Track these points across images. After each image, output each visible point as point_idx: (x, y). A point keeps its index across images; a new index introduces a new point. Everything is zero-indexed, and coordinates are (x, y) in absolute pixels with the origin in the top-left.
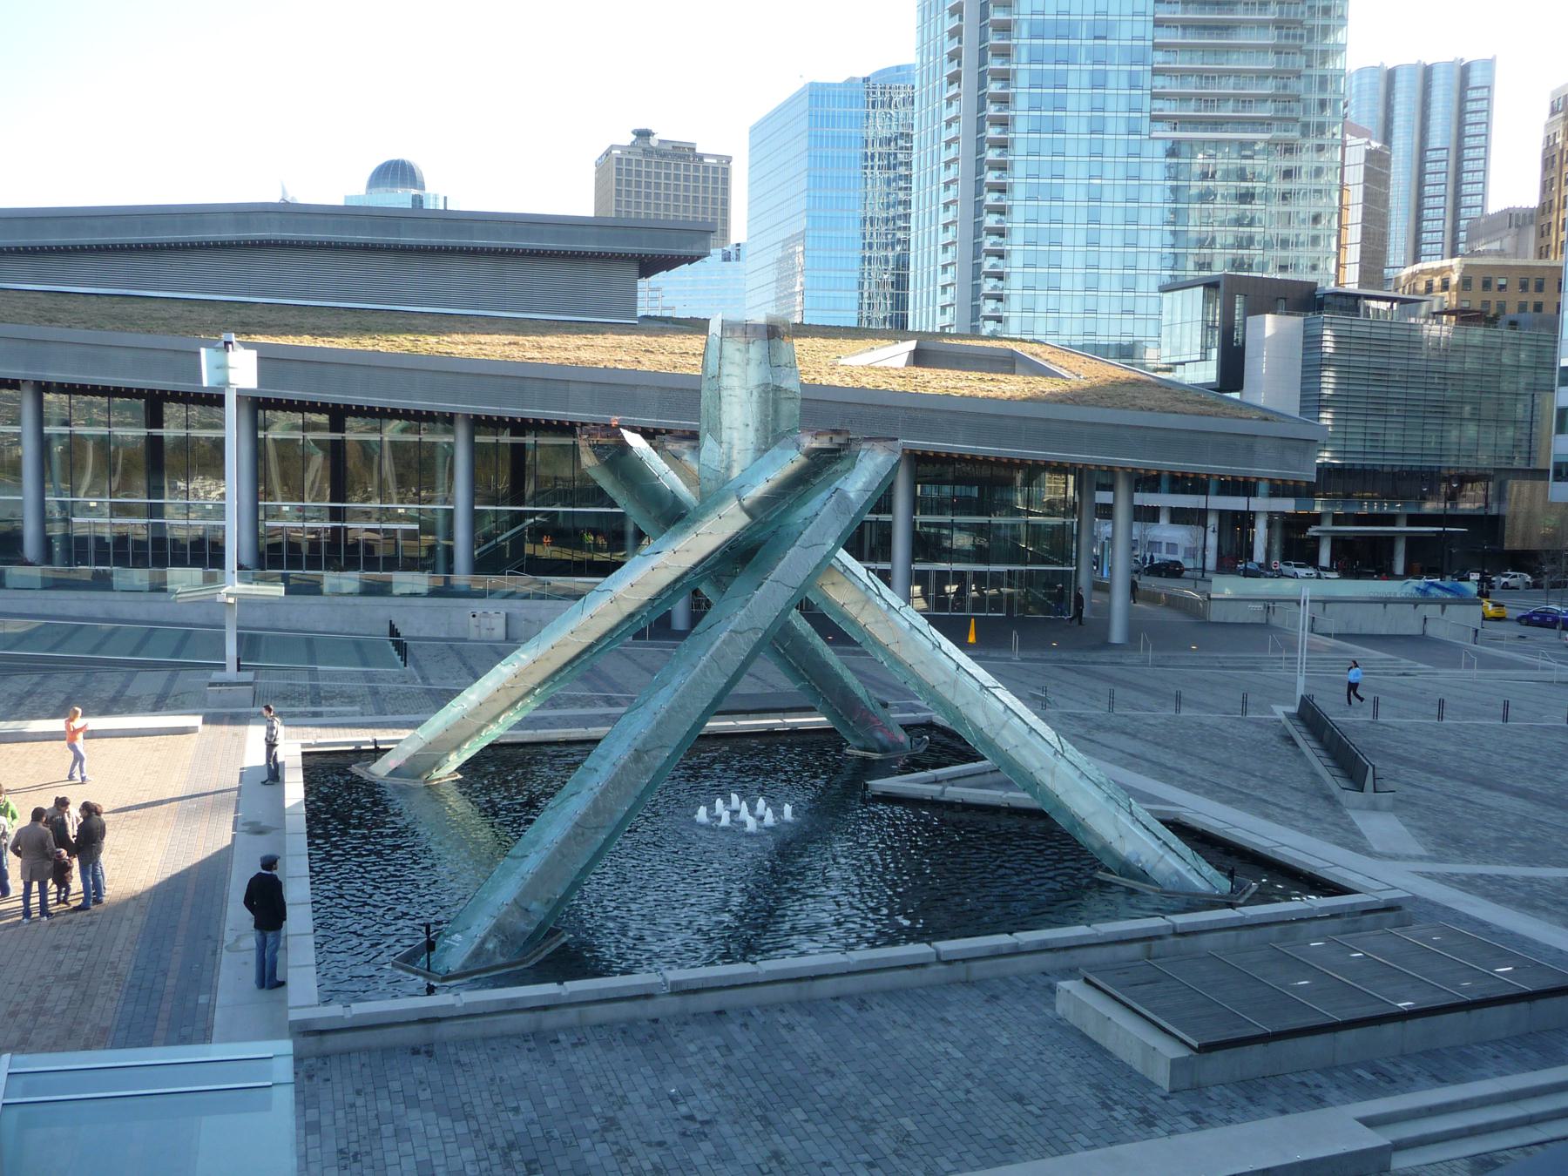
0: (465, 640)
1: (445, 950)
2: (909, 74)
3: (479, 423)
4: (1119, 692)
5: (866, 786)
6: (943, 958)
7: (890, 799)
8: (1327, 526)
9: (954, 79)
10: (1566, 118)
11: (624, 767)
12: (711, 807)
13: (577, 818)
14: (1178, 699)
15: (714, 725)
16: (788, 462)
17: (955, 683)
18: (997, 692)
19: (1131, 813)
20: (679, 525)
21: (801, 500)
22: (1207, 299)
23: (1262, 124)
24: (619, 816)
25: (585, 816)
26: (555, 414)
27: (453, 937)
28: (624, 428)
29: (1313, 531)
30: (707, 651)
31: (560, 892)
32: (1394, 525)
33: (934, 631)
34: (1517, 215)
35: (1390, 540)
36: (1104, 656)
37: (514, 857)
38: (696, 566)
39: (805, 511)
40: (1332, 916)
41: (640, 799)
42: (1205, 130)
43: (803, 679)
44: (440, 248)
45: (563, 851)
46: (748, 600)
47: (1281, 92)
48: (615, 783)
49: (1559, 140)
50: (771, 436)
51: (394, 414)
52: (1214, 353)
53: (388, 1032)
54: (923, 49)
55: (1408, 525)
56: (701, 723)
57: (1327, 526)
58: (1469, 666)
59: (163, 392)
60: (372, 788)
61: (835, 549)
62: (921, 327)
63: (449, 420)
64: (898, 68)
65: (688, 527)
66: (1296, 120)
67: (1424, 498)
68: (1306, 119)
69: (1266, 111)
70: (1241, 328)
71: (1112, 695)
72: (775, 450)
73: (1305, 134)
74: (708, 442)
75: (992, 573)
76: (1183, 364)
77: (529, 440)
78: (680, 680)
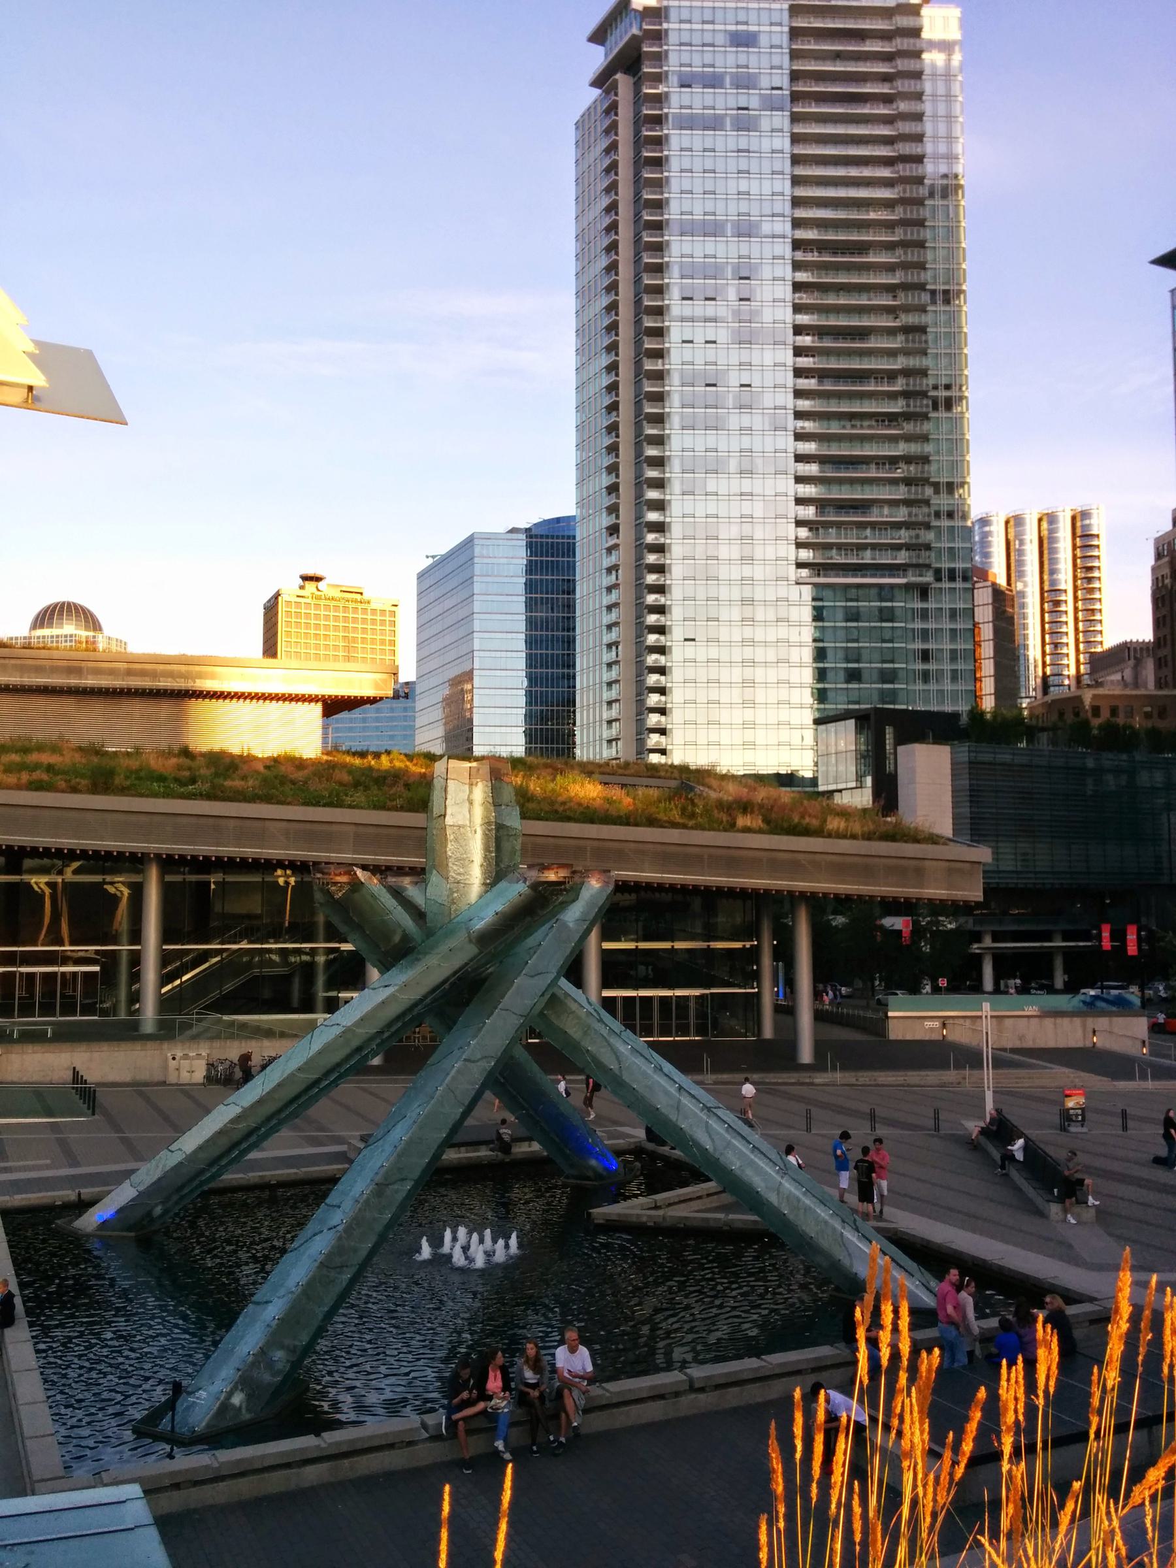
0: (164, 1083)
1: (188, 1408)
2: (569, 525)
3: (168, 863)
4: (815, 1111)
5: (589, 1214)
6: (697, 1385)
7: (613, 1227)
8: (988, 942)
9: (613, 530)
10: (1171, 563)
11: (367, 1202)
12: (437, 1242)
13: (321, 1258)
14: (872, 1117)
15: (452, 1156)
16: (514, 891)
17: (678, 1107)
18: (720, 1112)
19: (857, 1230)
20: (409, 958)
21: (529, 931)
22: (859, 730)
23: (898, 570)
24: (363, 1253)
25: (330, 1256)
26: (250, 851)
27: (197, 1394)
28: (356, 865)
29: (975, 948)
30: (443, 1081)
31: (304, 1338)
32: (1051, 941)
33: (655, 1054)
34: (1135, 649)
35: (1049, 955)
36: (792, 1077)
37: (258, 1303)
38: (425, 997)
39: (531, 941)
40: (653, 1398)
41: (382, 1238)
42: (837, 576)
43: (523, 1108)
44: (122, 690)
45: (309, 1290)
46: (480, 1030)
47: (914, 541)
48: (356, 1224)
49: (1167, 581)
50: (497, 874)
51: (71, 855)
52: (869, 780)
53: (634, 1409)
54: (580, 504)
55: (1064, 940)
56: (437, 1156)
57: (988, 942)
58: (1143, 1077)
59: (22, 848)
60: (77, 1240)
61: (557, 979)
62: (595, 755)
63: (135, 862)
64: (558, 520)
65: (418, 960)
66: (928, 566)
67: (548, 868)
68: (938, 565)
69: (902, 558)
70: (892, 757)
71: (809, 1117)
72: (503, 885)
73: (938, 579)
74: (434, 878)
75: (641, 997)
76: (840, 791)
77: (214, 879)
78: (417, 1111)
